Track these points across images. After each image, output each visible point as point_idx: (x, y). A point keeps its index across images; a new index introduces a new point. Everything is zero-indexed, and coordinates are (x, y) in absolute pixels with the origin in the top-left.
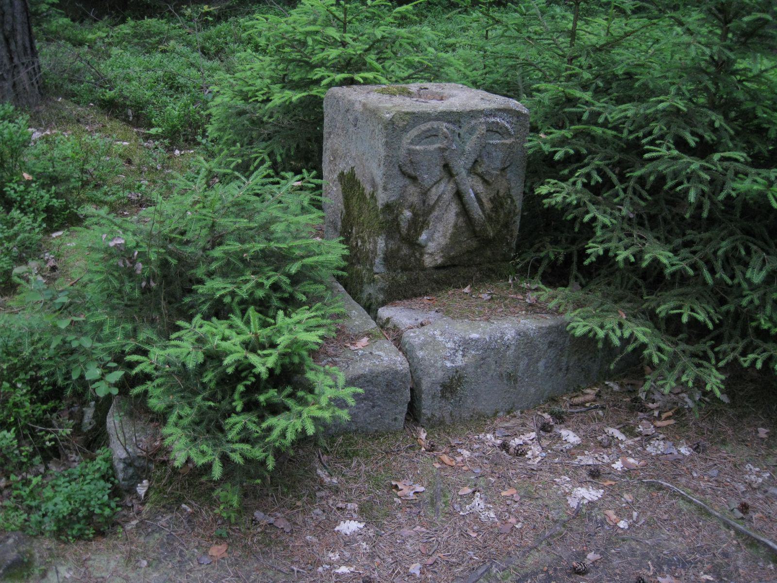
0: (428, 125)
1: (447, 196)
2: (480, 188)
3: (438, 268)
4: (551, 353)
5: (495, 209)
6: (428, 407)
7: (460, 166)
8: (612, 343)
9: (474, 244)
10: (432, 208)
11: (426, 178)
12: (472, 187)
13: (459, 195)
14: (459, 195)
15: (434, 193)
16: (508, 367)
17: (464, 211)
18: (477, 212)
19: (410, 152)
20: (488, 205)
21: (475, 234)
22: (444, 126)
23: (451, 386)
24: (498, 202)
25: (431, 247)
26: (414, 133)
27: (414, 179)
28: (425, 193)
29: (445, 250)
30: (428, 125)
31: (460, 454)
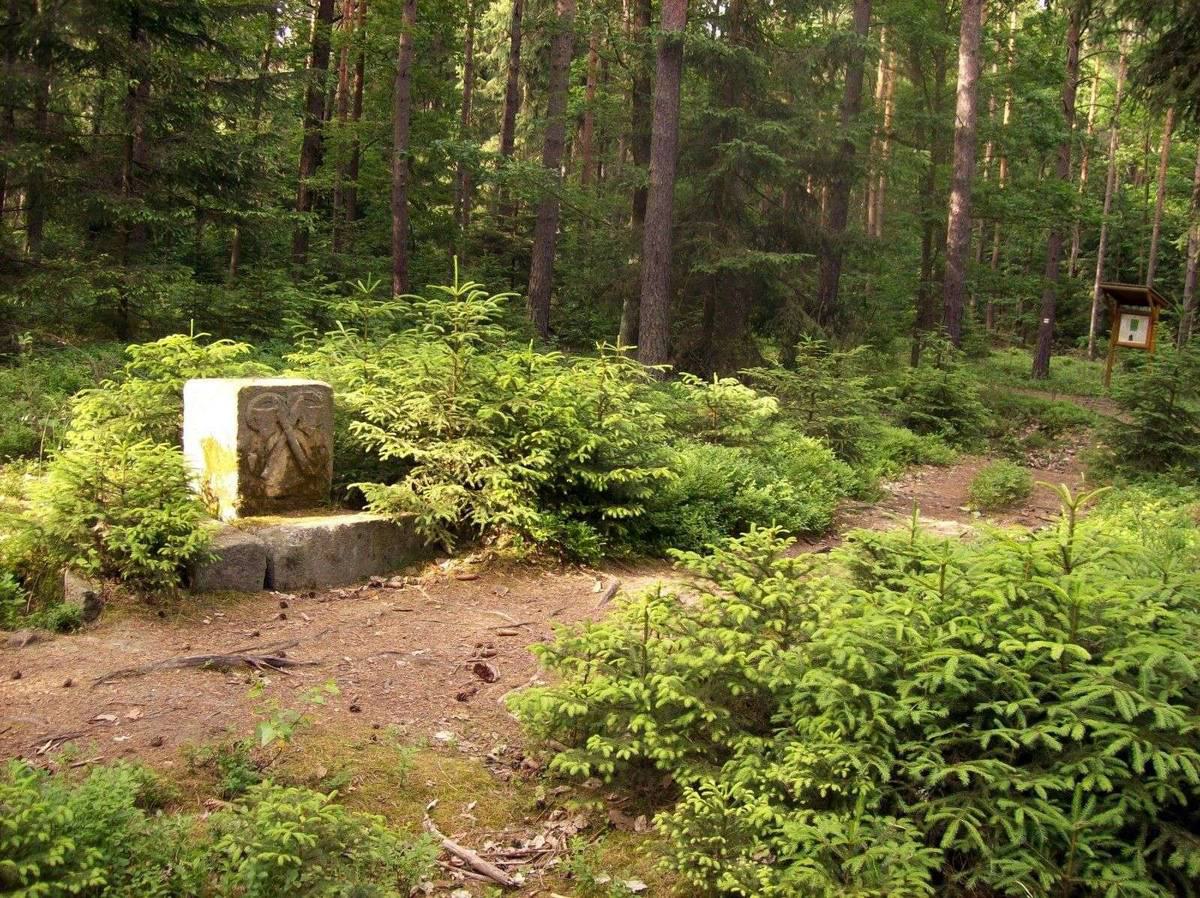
0: (262, 396)
1: (282, 444)
2: (303, 439)
3: (277, 498)
4: (362, 542)
5: (314, 455)
6: (279, 576)
7: (288, 424)
8: (970, 62)
9: (302, 479)
10: (270, 453)
11: (265, 430)
12: (298, 438)
13: (288, 444)
14: (288, 444)
15: (272, 441)
16: (331, 550)
17: (293, 456)
18: (301, 456)
19: (254, 412)
20: (309, 452)
21: (301, 473)
22: (276, 397)
23: (293, 561)
24: (316, 449)
25: (272, 481)
26: (255, 400)
27: (257, 431)
28: (265, 441)
29: (282, 484)
30: (262, 396)
31: (476, 217)
